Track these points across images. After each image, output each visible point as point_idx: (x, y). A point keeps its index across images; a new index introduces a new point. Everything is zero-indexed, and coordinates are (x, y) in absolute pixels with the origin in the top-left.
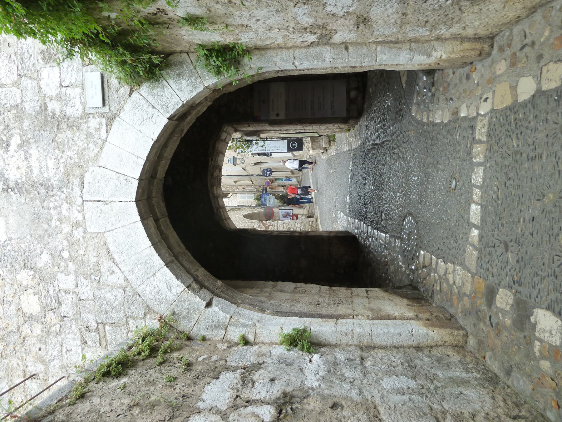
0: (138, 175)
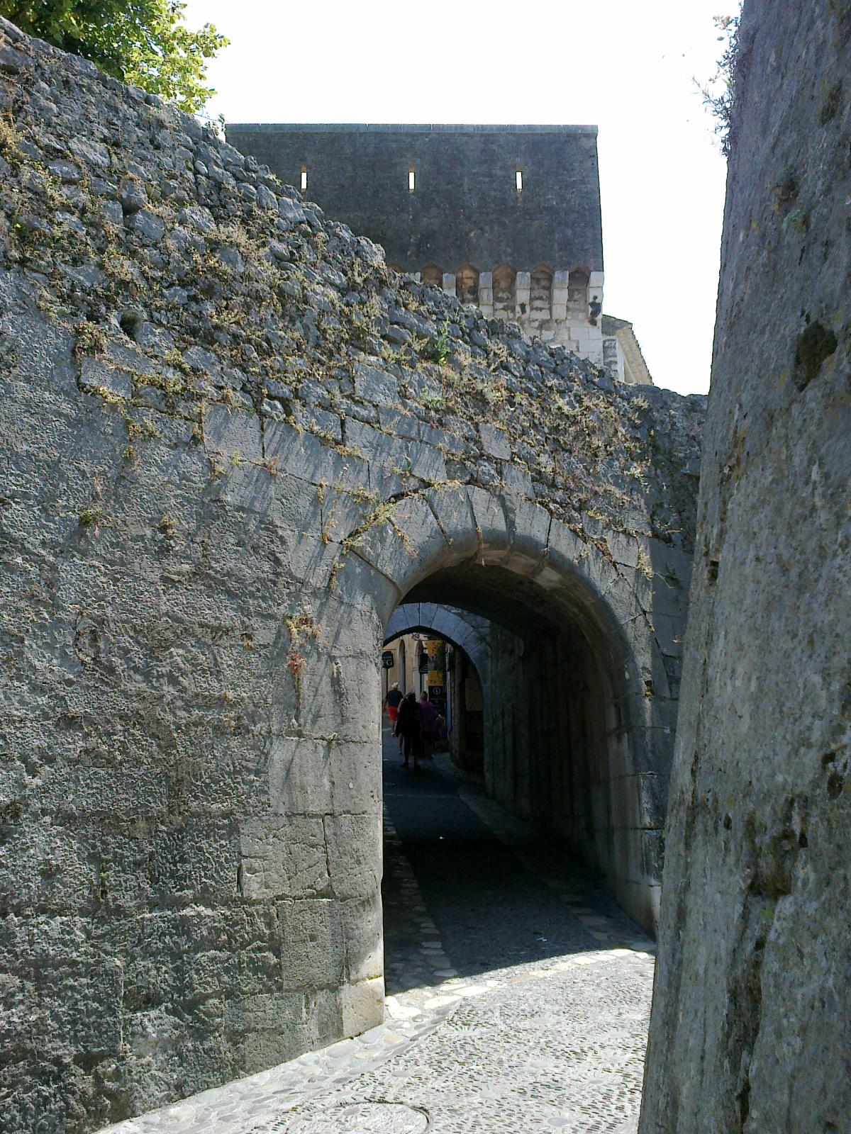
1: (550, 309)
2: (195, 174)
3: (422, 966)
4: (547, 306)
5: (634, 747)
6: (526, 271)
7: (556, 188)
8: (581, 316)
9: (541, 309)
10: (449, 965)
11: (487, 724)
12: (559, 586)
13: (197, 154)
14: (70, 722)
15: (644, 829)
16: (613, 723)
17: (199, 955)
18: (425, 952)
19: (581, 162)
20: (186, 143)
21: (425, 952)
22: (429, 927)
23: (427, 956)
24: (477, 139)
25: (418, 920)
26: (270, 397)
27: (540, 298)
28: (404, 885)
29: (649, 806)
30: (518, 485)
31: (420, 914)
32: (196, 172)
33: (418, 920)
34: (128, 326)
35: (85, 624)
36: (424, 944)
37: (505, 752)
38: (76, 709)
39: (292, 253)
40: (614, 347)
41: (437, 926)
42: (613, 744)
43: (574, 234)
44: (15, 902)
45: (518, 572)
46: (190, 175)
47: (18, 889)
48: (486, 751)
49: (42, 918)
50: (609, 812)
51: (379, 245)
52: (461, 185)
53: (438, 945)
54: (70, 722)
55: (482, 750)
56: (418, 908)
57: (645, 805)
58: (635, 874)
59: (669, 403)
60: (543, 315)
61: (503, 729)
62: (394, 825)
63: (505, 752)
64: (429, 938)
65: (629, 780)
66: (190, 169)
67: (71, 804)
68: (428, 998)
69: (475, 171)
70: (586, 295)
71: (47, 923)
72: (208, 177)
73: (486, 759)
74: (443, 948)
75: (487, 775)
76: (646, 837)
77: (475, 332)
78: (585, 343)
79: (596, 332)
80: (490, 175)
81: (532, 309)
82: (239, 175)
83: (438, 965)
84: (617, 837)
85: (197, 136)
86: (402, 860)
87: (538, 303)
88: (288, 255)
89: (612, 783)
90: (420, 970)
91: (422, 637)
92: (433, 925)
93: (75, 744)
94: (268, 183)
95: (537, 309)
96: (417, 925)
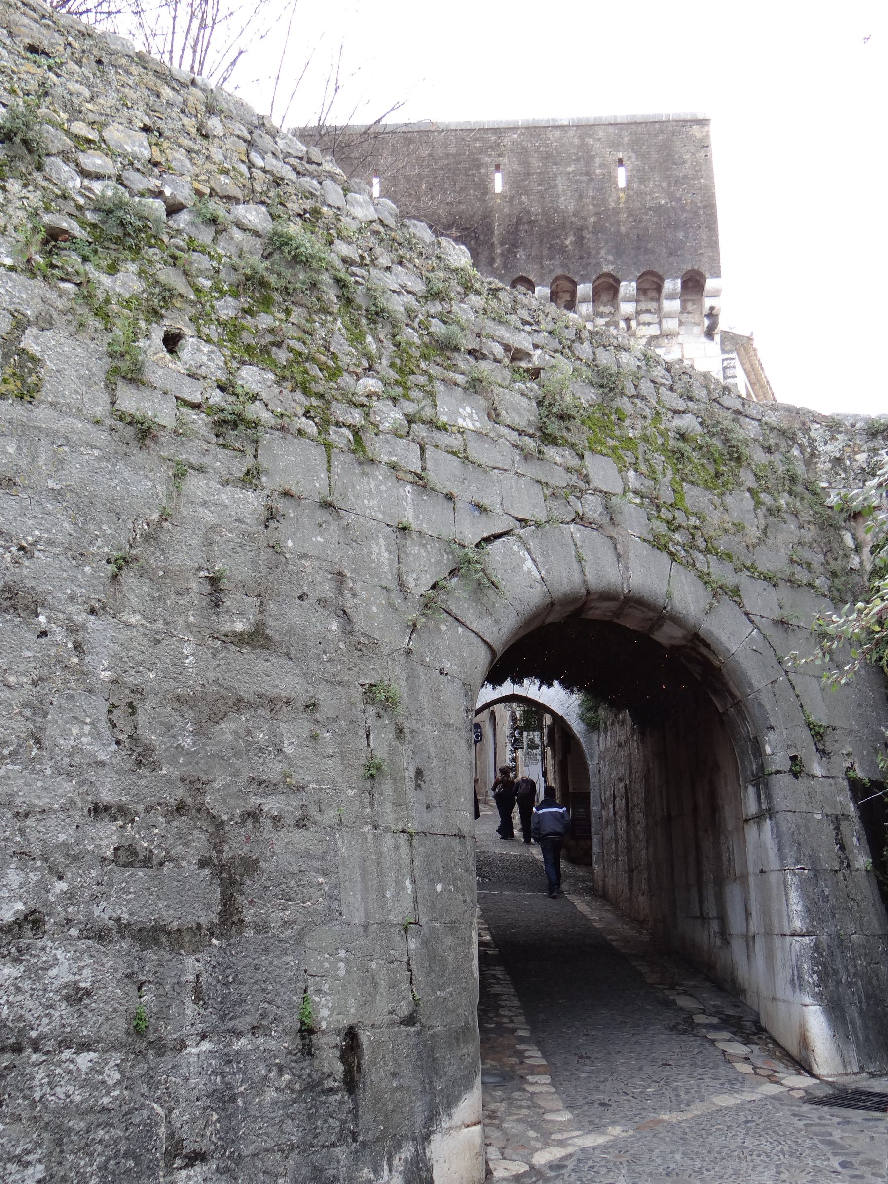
0: (529, 696)
1: (660, 323)
2: (249, 168)
3: (529, 1107)
4: (657, 320)
5: (778, 834)
6: (631, 281)
7: (665, 184)
8: (697, 330)
9: (649, 324)
10: (560, 1105)
11: (595, 808)
12: (683, 643)
13: (250, 144)
14: (98, 810)
15: (793, 935)
16: (752, 807)
17: (382, 541)
18: (531, 1089)
19: (693, 154)
20: (238, 133)
21: (531, 1089)
22: (534, 1056)
23: (533, 1094)
24: (572, 133)
25: (520, 1047)
26: (337, 424)
27: (648, 311)
28: (503, 1004)
29: (799, 908)
30: (635, 523)
31: (522, 1040)
32: (251, 166)
33: (520, 1047)
34: (172, 342)
35: (122, 698)
36: (530, 1078)
37: (617, 841)
38: (106, 796)
39: (362, 258)
40: (734, 367)
41: (545, 1056)
42: (751, 832)
43: (686, 237)
44: (33, 1034)
45: (634, 628)
46: (243, 168)
47: (37, 1018)
48: (595, 839)
49: (67, 1054)
50: (748, 914)
51: (463, 247)
52: (556, 186)
53: (546, 1079)
54: (98, 810)
55: (590, 838)
56: (521, 1033)
57: (794, 907)
58: (783, 990)
59: (809, 424)
60: (654, 330)
61: (615, 815)
62: (488, 929)
63: (617, 841)
64: (534, 1070)
65: (773, 878)
66: (243, 162)
67: (103, 913)
68: (537, 1150)
69: (570, 169)
70: (701, 304)
71: (72, 1061)
72: (265, 171)
73: (595, 849)
74: (553, 1084)
75: (596, 867)
76: (796, 946)
77: (577, 344)
78: (703, 356)
79: (714, 347)
80: (587, 173)
81: (639, 324)
82: (300, 169)
83: (548, 1105)
84: (759, 946)
85: (251, 124)
86: (499, 972)
87: (646, 318)
88: (358, 260)
89: (752, 880)
90: (525, 1111)
91: (514, 705)
92: (539, 1054)
93: (106, 836)
94: (333, 177)
95: (644, 324)
96: (520, 1054)
